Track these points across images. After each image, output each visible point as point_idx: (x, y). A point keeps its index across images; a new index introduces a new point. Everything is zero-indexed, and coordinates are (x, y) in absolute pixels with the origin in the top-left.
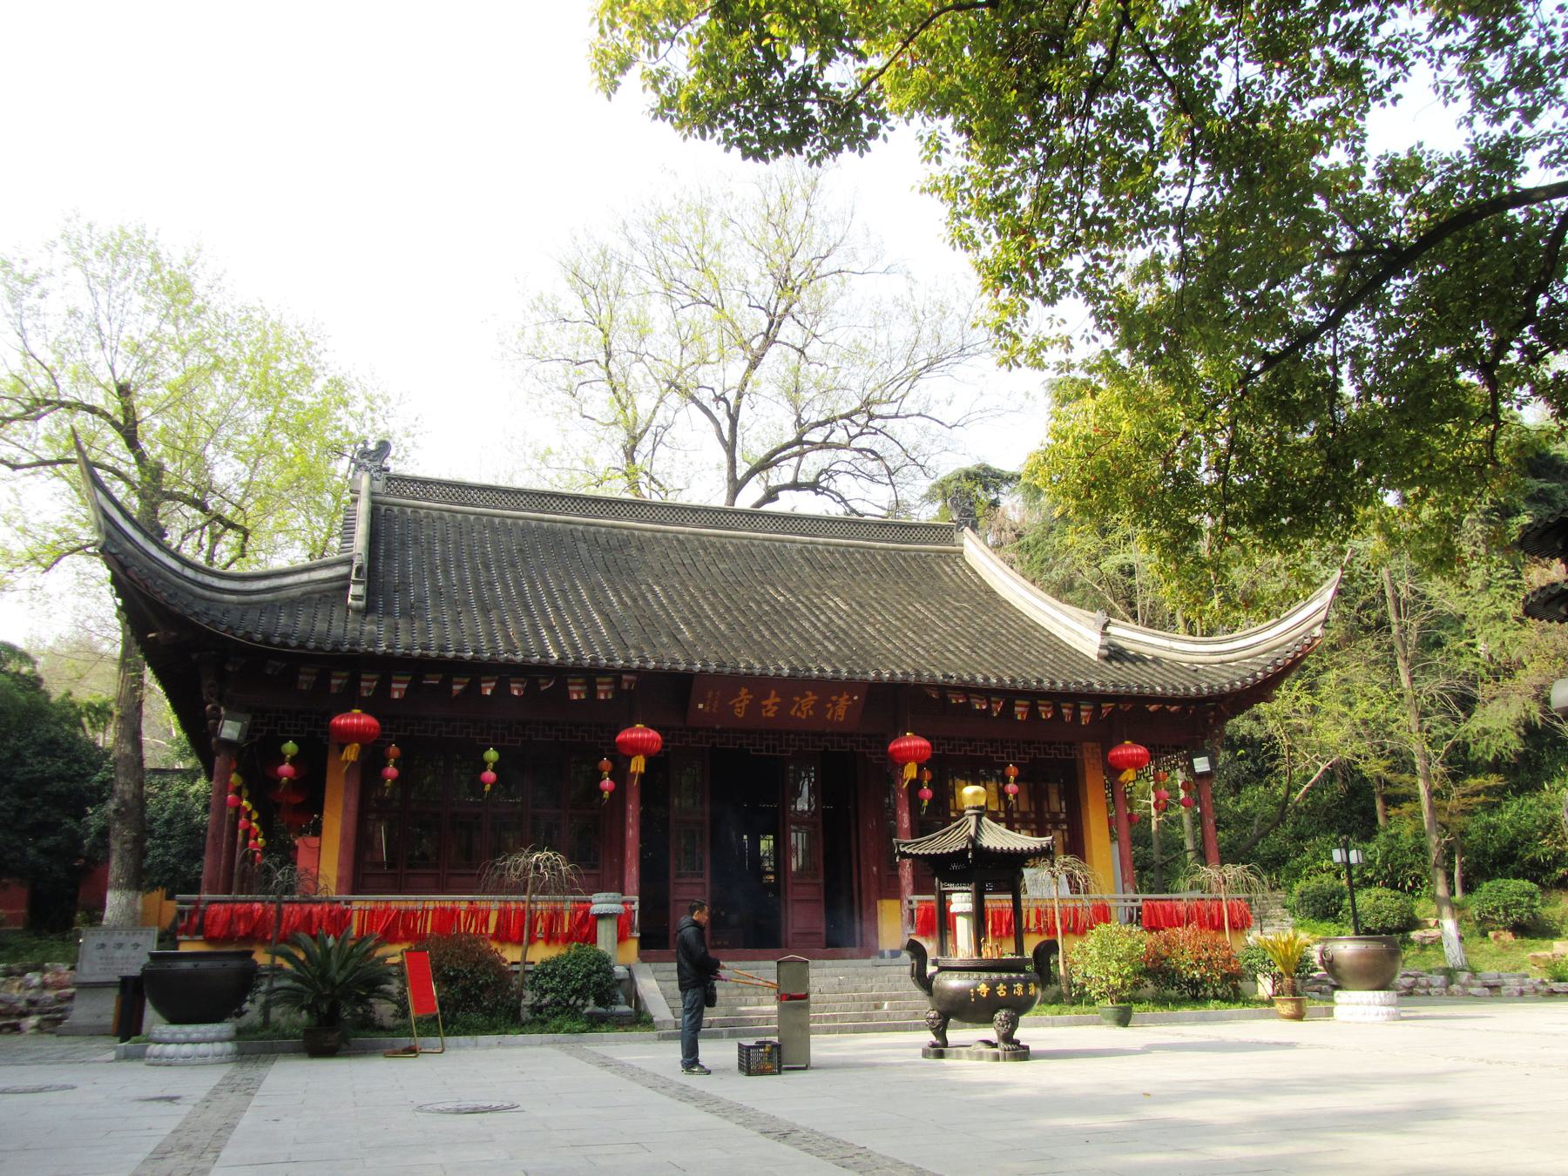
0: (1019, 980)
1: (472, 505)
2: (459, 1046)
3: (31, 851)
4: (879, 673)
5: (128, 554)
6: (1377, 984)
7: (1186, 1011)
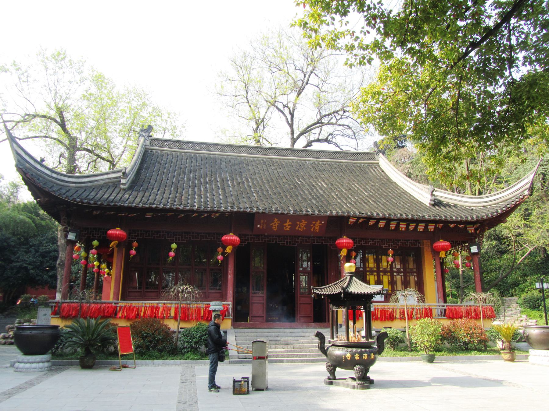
0: (366, 352)
1: (183, 149)
2: (142, 365)
3: (45, 276)
4: (331, 212)
5: (27, 169)
6: (546, 348)
7: (461, 355)
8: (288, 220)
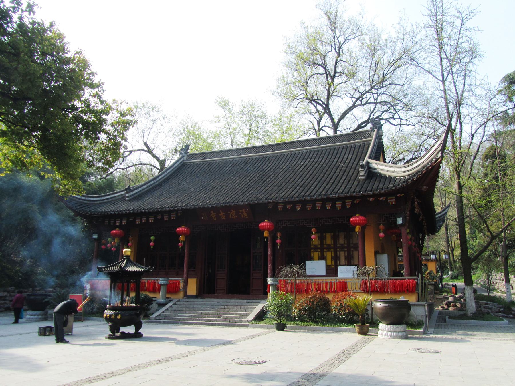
6: (388, 322)
8: (221, 212)
